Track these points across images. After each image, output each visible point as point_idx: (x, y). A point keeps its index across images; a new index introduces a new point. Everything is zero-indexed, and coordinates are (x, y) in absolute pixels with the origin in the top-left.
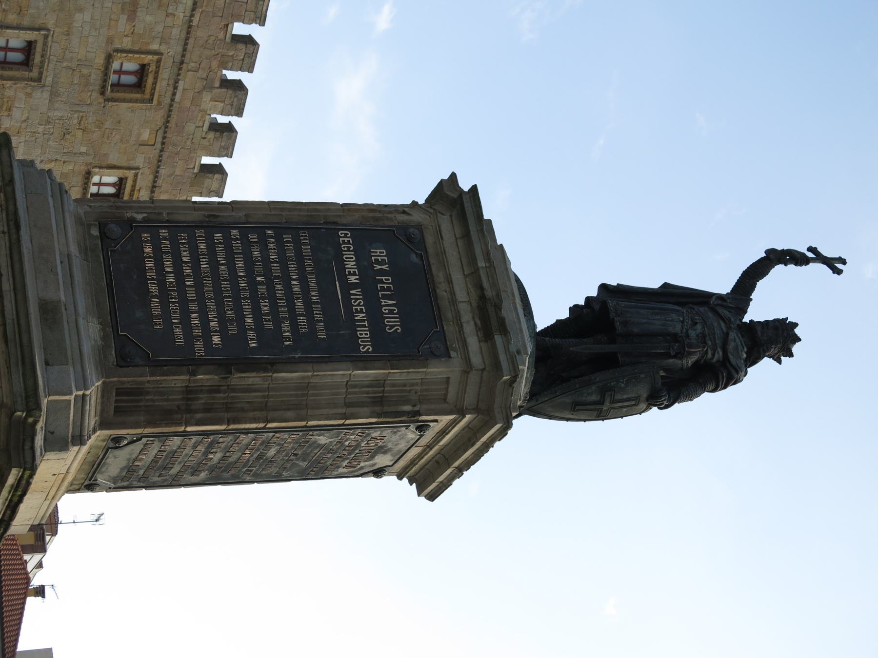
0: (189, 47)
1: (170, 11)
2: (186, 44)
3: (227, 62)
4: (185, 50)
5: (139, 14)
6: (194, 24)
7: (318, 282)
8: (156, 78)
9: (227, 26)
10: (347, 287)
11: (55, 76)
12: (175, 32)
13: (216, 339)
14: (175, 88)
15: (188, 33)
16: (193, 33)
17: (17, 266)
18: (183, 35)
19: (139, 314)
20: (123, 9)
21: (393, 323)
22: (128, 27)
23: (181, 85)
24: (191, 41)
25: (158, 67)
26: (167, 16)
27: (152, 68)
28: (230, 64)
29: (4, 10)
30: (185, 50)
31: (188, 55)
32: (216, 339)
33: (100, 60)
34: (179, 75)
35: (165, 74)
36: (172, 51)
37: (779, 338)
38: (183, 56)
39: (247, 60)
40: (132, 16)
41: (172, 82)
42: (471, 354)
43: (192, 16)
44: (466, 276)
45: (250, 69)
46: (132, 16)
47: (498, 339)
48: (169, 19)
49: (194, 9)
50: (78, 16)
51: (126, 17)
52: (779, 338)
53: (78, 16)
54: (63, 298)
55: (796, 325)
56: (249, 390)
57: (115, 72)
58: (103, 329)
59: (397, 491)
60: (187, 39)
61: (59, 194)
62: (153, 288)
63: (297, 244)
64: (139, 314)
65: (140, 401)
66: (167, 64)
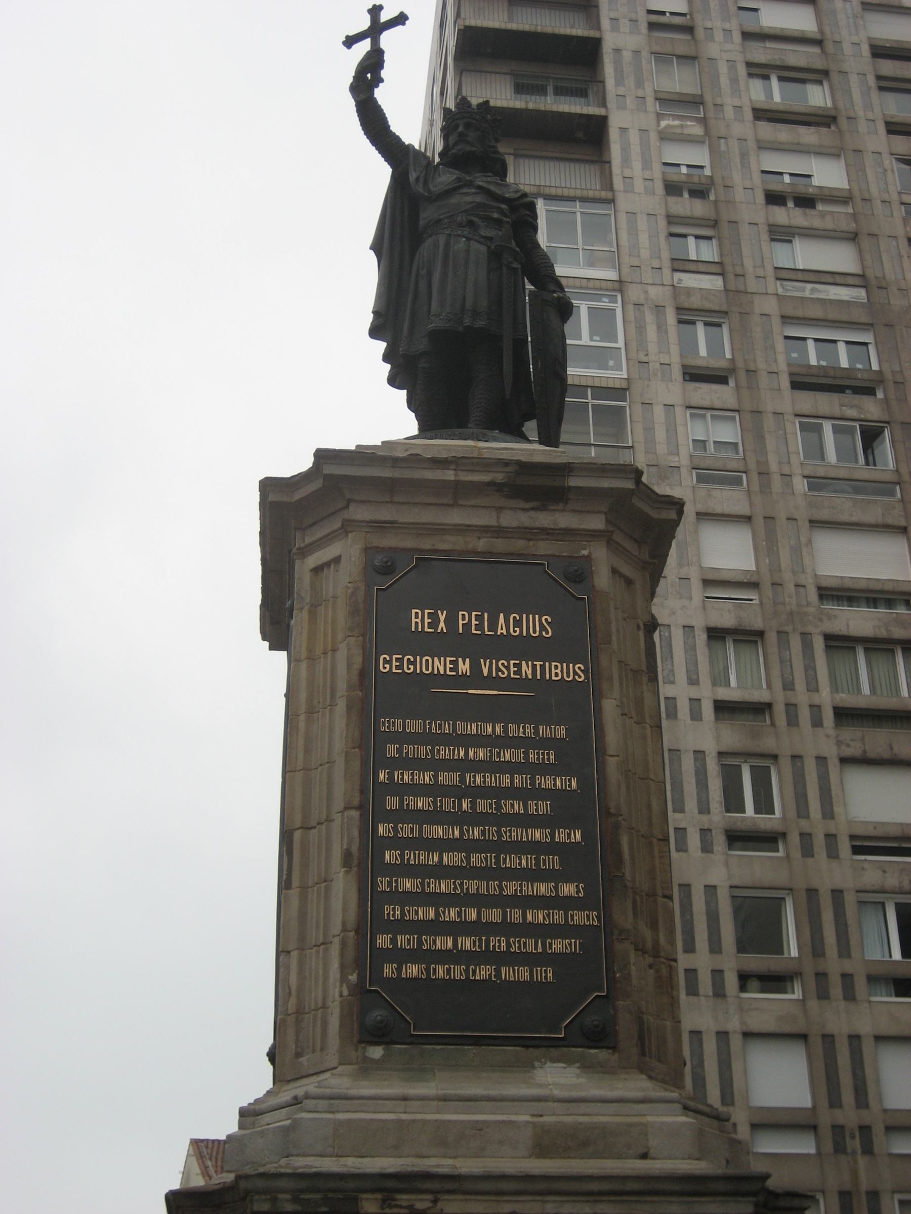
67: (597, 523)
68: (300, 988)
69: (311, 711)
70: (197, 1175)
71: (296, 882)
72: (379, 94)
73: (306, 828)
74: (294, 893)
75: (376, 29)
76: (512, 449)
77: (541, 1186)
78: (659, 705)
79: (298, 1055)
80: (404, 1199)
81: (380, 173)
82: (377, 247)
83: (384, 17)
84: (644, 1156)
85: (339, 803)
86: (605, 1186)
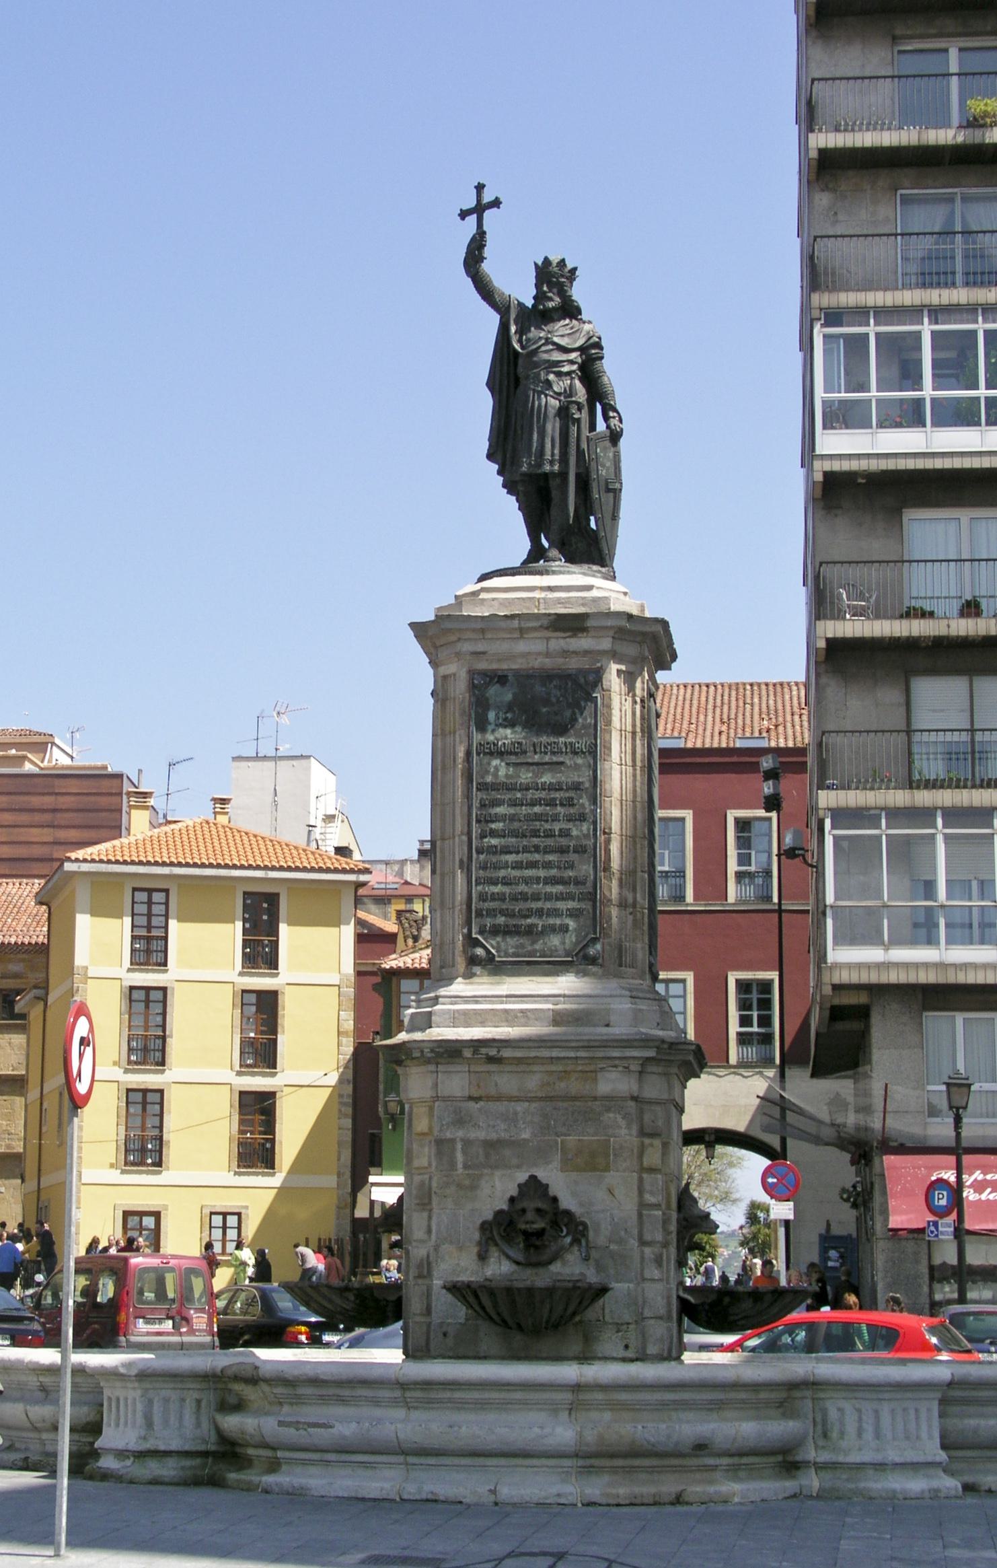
67: (606, 644)
68: (442, 931)
69: (444, 768)
70: (642, 608)
71: (438, 872)
72: (486, 266)
73: (443, 839)
74: (438, 877)
75: (479, 209)
76: (454, 821)
77: (549, 1044)
78: (814, 528)
79: (442, 967)
80: (483, 1051)
81: (493, 319)
82: (490, 384)
83: (487, 197)
84: (607, 1025)
85: (458, 832)
86: (581, 1044)
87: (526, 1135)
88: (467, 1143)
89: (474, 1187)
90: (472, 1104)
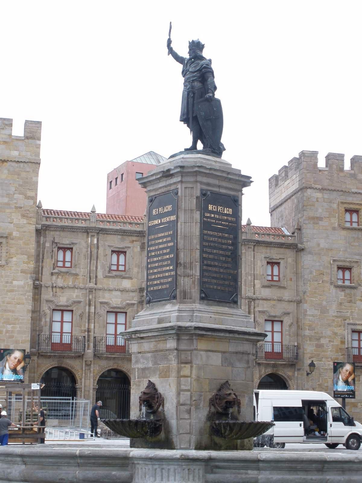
0: (333, 188)
1: (315, 200)
2: (332, 190)
3: (340, 168)
4: (335, 190)
5: (318, 216)
6: (320, 187)
7: (162, 233)
8: (352, 203)
9: (320, 171)
10: (161, 224)
11: (355, 255)
12: (326, 196)
13: (171, 268)
14: (356, 193)
15: (325, 189)
16: (326, 187)
17: (146, 331)
18: (328, 192)
19: (165, 292)
20: (317, 224)
21: (169, 208)
22: (326, 220)
23: (353, 190)
24: (330, 188)
25: (345, 203)
26: (318, 201)
27: (346, 206)
28: (341, 166)
29: (322, 282)
30: (335, 190)
31: (338, 189)
32: (171, 268)
33: (344, 233)
34: (349, 192)
35: (350, 199)
36: (338, 198)
37: (196, 47)
38: (338, 191)
39: (338, 158)
40: (320, 219)
41: (353, 195)
42: (177, 181)
43: (316, 188)
44: (160, 182)
45: (342, 156)
46: (320, 219)
47: (172, 172)
48: (319, 200)
49: (313, 188)
50: (322, 246)
51: (320, 222)
52: (196, 47)
53: (322, 246)
54: (158, 317)
55: (189, 42)
56: (195, 253)
57: (351, 225)
58: (169, 303)
59: (243, 196)
60: (328, 190)
61: (153, 313)
62: (160, 287)
63: (152, 240)
64: (165, 292)
65: (188, 291)
66: (343, 198)
87: (151, 366)
88: (138, 369)
89: (139, 385)
90: (140, 354)
